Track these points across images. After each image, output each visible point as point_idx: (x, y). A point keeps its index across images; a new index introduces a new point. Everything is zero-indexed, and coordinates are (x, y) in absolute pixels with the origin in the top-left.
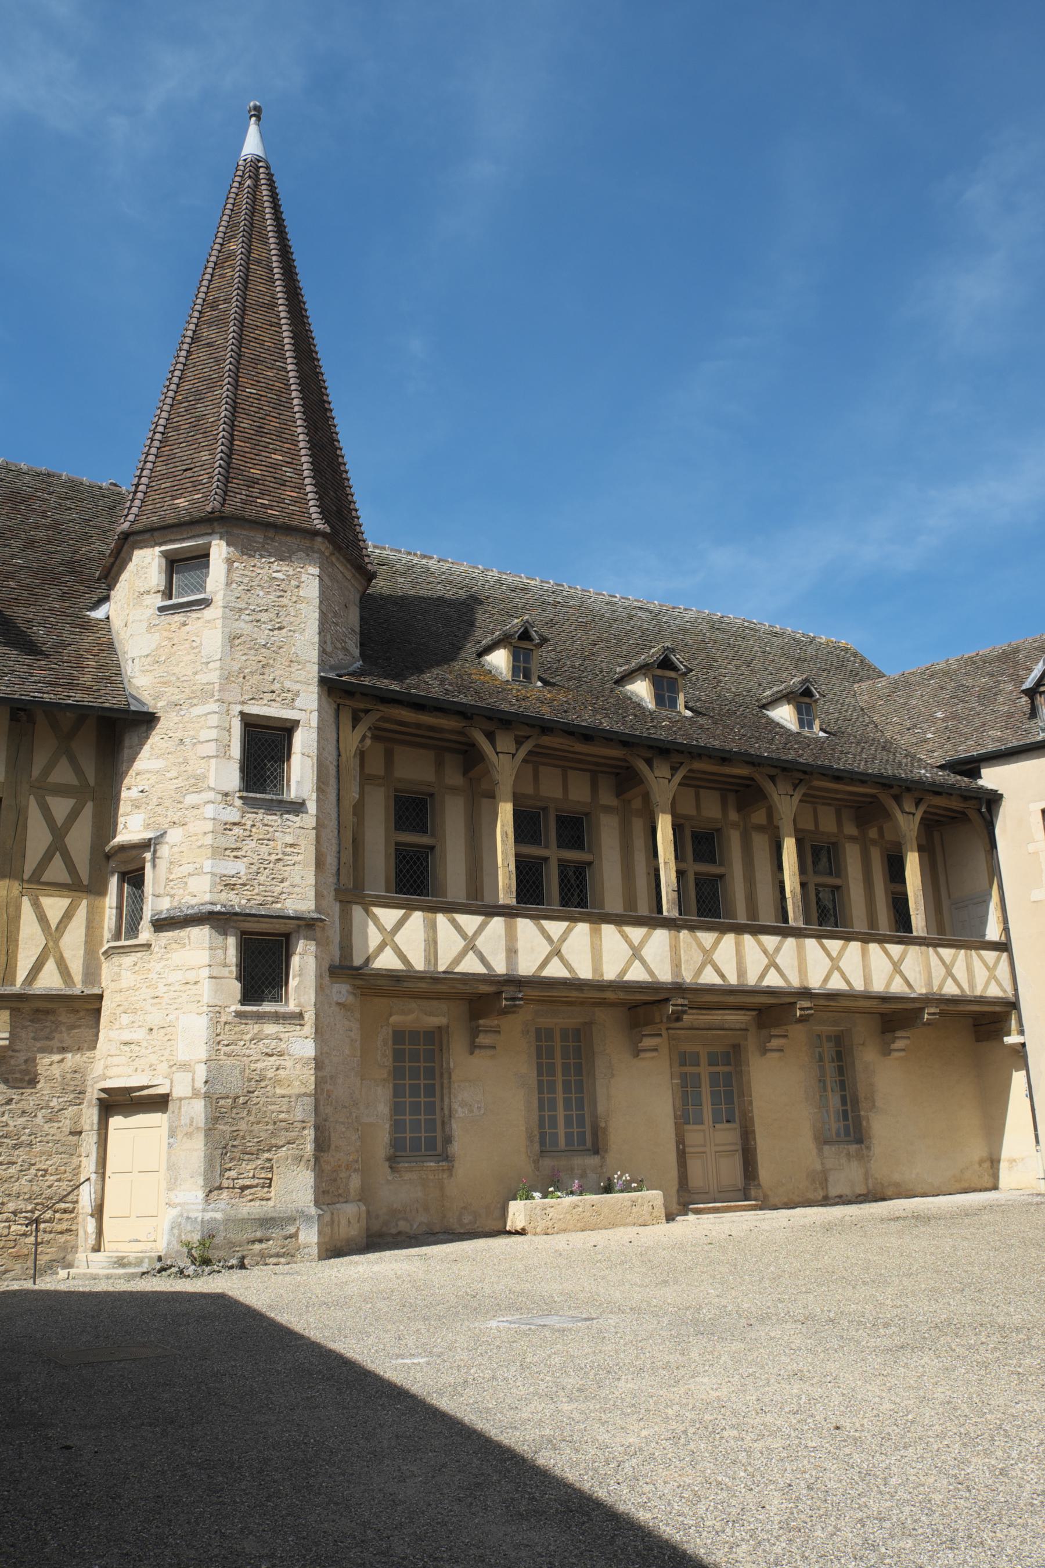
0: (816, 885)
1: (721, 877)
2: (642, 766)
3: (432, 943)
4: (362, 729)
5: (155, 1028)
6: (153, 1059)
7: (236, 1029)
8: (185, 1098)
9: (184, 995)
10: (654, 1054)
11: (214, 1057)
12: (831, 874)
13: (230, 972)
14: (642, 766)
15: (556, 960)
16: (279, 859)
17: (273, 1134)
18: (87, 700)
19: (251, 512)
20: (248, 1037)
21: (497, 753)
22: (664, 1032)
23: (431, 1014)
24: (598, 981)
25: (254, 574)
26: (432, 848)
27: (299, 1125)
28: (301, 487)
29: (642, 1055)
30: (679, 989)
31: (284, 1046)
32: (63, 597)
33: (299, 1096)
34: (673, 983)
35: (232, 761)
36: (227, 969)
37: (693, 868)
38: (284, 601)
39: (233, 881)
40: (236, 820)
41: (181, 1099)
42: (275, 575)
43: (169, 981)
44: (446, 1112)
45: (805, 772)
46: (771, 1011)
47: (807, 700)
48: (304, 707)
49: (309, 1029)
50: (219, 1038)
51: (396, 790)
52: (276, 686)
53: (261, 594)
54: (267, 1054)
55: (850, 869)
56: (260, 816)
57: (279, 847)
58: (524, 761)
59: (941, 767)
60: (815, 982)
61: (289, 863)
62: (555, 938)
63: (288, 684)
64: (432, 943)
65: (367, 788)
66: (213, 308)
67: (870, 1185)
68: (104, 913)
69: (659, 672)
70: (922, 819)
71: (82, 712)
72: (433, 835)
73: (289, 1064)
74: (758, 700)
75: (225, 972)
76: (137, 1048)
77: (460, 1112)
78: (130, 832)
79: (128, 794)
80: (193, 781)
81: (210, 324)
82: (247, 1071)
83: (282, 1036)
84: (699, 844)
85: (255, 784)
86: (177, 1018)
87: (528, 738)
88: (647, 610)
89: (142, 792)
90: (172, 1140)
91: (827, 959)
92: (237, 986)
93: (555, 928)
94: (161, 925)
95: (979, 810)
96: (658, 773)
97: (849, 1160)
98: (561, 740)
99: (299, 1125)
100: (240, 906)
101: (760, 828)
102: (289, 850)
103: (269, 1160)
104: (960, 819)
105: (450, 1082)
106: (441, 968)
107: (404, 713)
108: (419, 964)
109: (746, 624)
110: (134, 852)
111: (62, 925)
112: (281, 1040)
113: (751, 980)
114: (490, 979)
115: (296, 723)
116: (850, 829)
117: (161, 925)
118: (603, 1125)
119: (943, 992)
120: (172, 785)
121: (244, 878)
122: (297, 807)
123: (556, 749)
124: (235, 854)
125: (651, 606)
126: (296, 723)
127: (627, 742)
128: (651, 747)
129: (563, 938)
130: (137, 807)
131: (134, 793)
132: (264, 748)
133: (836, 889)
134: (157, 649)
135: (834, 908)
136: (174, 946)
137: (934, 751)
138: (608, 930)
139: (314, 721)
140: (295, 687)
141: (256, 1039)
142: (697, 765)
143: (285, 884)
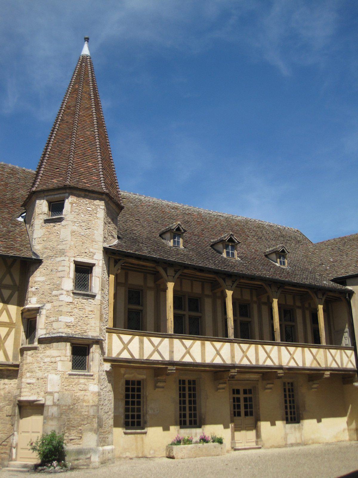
0: (285, 325)
1: (250, 322)
2: (221, 281)
3: (141, 348)
4: (118, 266)
5: (40, 379)
6: (38, 390)
7: (69, 380)
8: (50, 406)
9: (51, 367)
10: (224, 390)
11: (61, 391)
12: (291, 321)
13: (68, 359)
14: (221, 281)
15: (188, 355)
16: (87, 316)
17: (82, 420)
18: (17, 254)
19: (80, 186)
20: (74, 383)
21: (168, 276)
22: (227, 382)
23: (140, 374)
24: (204, 363)
25: (80, 208)
26: (142, 311)
27: (92, 417)
28: (98, 175)
29: (219, 391)
30: (234, 367)
31: (87, 387)
32: (9, 213)
33: (92, 406)
34: (231, 364)
35: (70, 279)
36: (66, 358)
37: (240, 319)
38: (91, 218)
39: (69, 324)
40: (71, 301)
41: (49, 406)
42: (88, 209)
43: (45, 361)
44: (145, 411)
45: (282, 283)
46: (267, 374)
47: (283, 254)
48: (98, 261)
49: (96, 381)
50: (63, 384)
51: (129, 288)
52: (87, 251)
53: (83, 216)
54: (80, 390)
55: (298, 319)
56: (80, 300)
57: (87, 312)
58: (178, 278)
59: (332, 281)
60: (284, 364)
61: (90, 318)
62: (188, 347)
63: (91, 250)
64: (141, 348)
65: (118, 288)
66: (69, 109)
67: (303, 439)
68: (20, 333)
69: (227, 243)
70: (325, 300)
71: (15, 259)
72: (142, 306)
73: (88, 394)
74: (265, 253)
75: (66, 359)
76: (33, 386)
77: (150, 412)
78: (31, 304)
79: (31, 289)
80: (56, 286)
81: (67, 115)
82: (73, 396)
83: (86, 383)
84: (241, 309)
85: (78, 287)
86: (48, 375)
87: (179, 270)
88: (223, 216)
89: (36, 289)
90: (45, 421)
91: (184, 348)
92: (71, 363)
93: (188, 343)
94: (42, 341)
95: (345, 297)
96: (227, 284)
97: (295, 430)
98: (192, 271)
99: (92, 417)
100: (72, 334)
101: (265, 303)
102: (90, 313)
103: (81, 430)
104: (337, 299)
105: (146, 401)
106: (145, 358)
107: (133, 260)
108: (137, 356)
109: (260, 222)
110: (33, 312)
111: (6, 338)
112: (86, 385)
113: (261, 363)
114: (164, 363)
115: (94, 265)
116: (298, 304)
117: (42, 341)
118: (203, 417)
119: (331, 367)
120: (48, 287)
121: (74, 323)
122: (93, 296)
123: (188, 274)
124: (71, 314)
125: (224, 215)
126: (94, 265)
127: (216, 272)
128: (225, 274)
129: (191, 347)
130: (35, 295)
131: (33, 289)
132: (83, 271)
133: (293, 326)
134: (44, 235)
135: (292, 334)
136: (47, 348)
137: (330, 274)
138: (208, 343)
139: (101, 264)
140: (94, 251)
141: (78, 384)
142: (242, 281)
143: (88, 326)
